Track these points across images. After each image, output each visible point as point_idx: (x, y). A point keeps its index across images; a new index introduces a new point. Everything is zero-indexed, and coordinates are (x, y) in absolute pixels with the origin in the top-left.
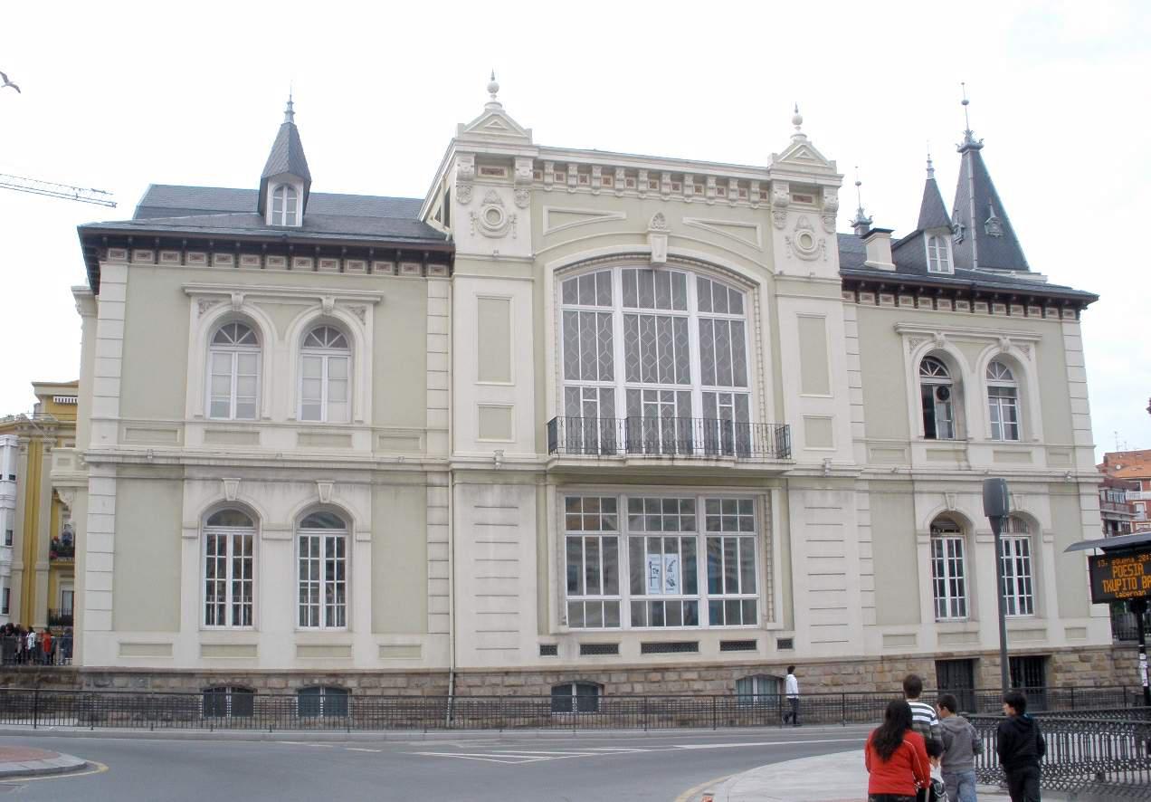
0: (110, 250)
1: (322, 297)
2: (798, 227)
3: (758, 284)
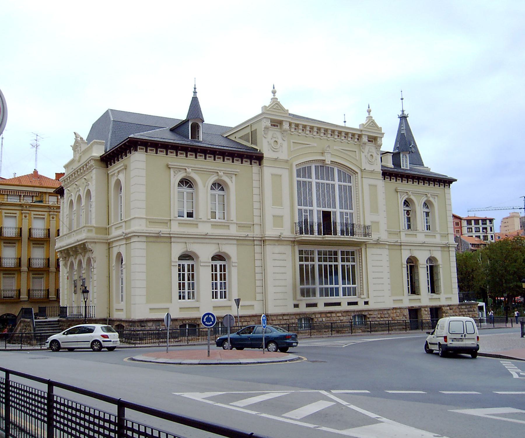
2: (273, 137)
3: (357, 173)
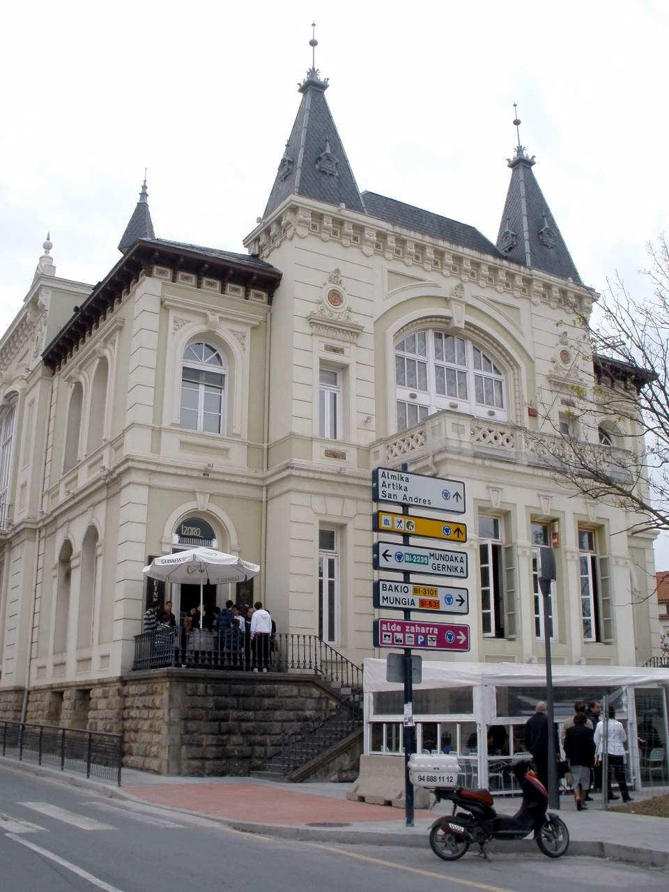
0: (156, 268)
1: (208, 313)
